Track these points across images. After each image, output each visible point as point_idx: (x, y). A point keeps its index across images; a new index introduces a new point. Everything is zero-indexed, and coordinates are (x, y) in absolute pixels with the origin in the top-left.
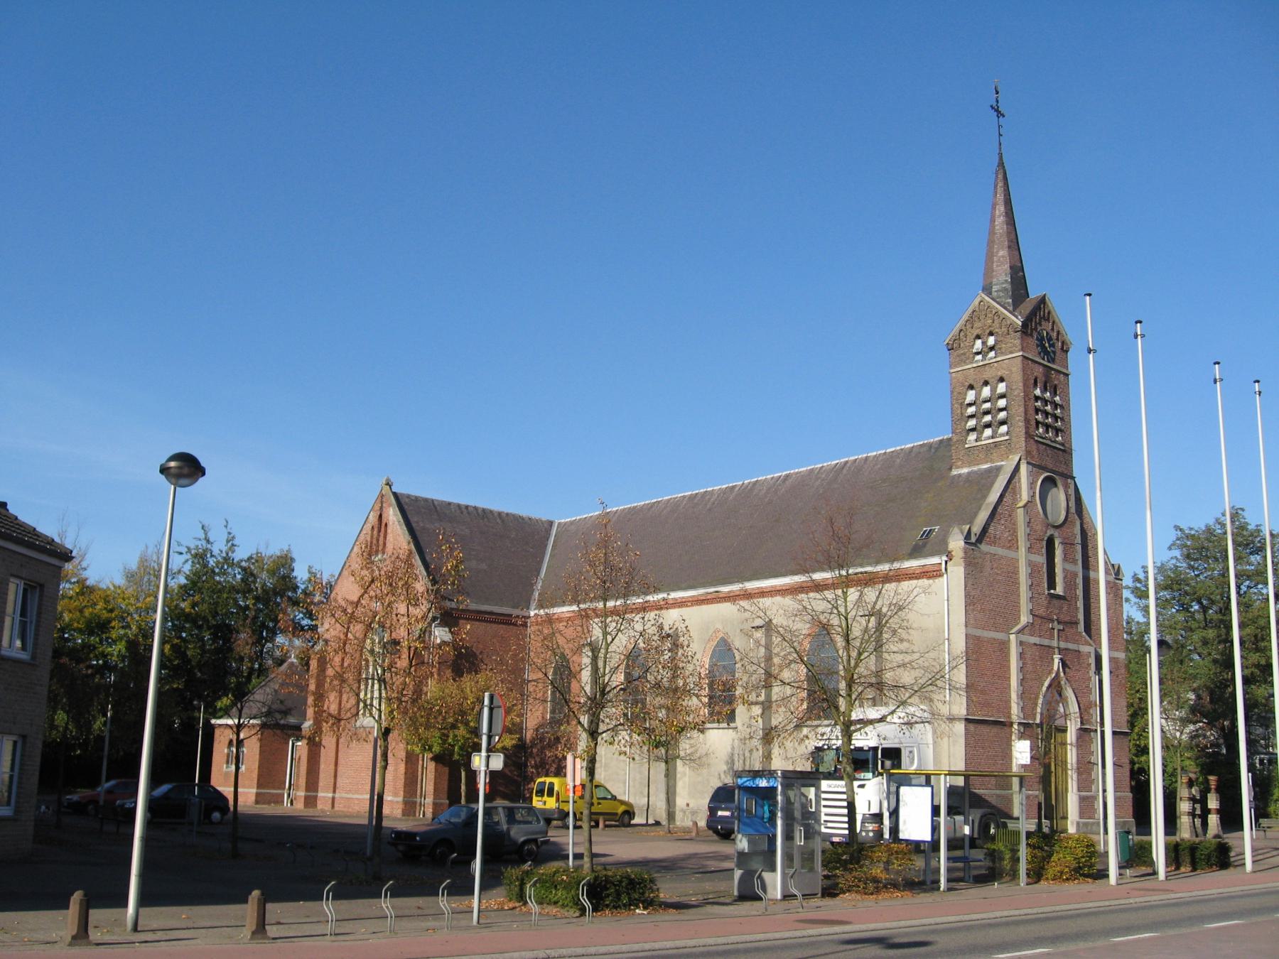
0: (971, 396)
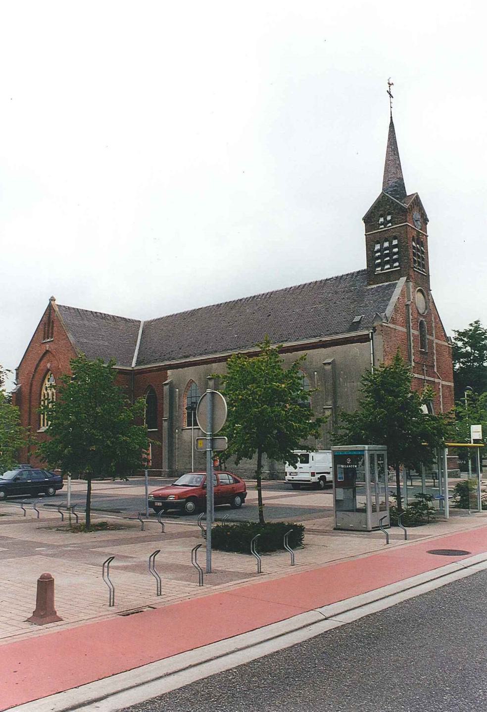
0: (378, 247)
